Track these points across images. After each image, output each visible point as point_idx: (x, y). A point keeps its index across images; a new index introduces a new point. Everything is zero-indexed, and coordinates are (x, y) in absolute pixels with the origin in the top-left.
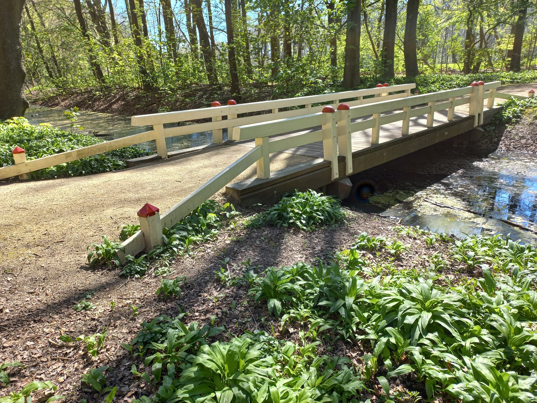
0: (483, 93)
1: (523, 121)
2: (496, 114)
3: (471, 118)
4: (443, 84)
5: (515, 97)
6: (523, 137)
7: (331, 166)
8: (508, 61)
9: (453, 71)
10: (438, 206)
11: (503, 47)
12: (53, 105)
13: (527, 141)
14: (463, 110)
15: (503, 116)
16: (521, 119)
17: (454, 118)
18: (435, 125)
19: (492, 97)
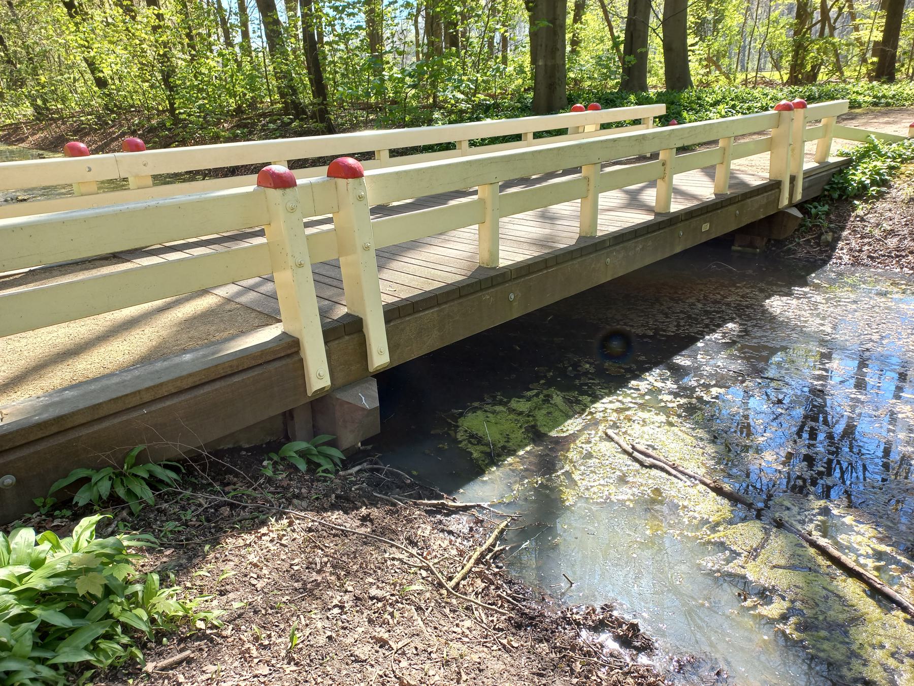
0: (804, 126)
1: (894, 192)
2: (833, 175)
3: (774, 186)
4: (734, 107)
5: (879, 136)
6: (891, 233)
7: (364, 330)
8: (872, 63)
9: (770, 84)
10: (636, 460)
11: (864, 35)
12: (17, 141)
13: (900, 241)
14: (754, 169)
15: (848, 181)
16: (890, 187)
17: (730, 187)
18: (677, 206)
19: (826, 135)
